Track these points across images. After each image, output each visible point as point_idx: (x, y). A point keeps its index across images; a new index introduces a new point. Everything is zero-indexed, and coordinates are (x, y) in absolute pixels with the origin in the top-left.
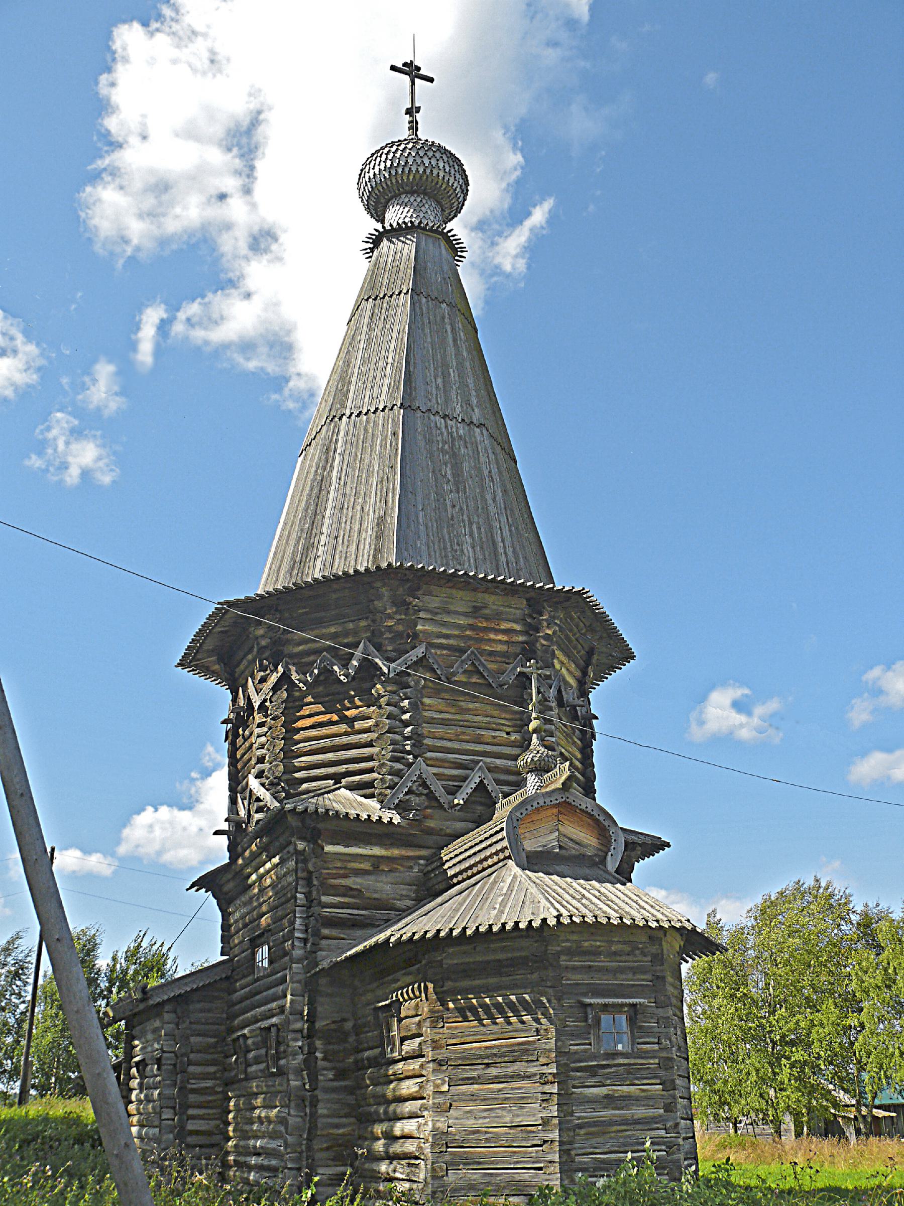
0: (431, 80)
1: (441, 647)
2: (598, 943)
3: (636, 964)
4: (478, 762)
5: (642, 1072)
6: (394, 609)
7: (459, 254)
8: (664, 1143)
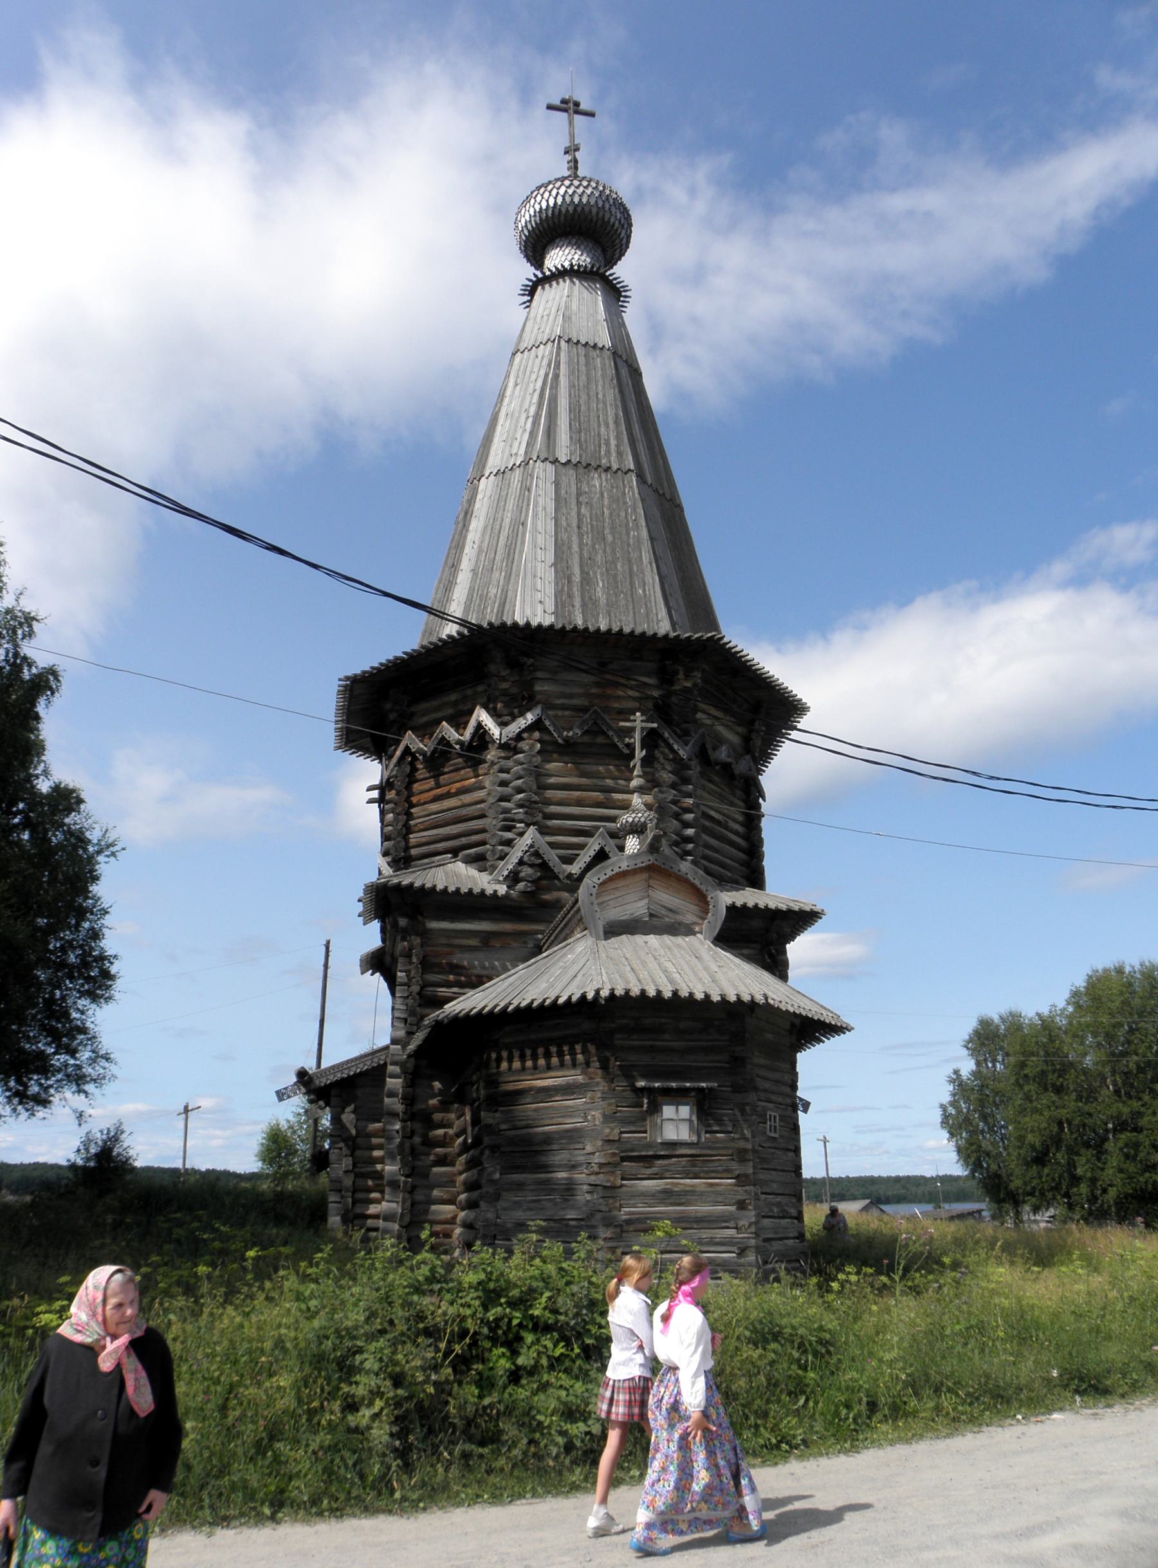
0: (592, 115)
1: (564, 708)
2: (663, 1020)
3: (710, 1043)
4: (598, 828)
5: (710, 1165)
6: (508, 672)
7: (623, 294)
8: (733, 1244)
